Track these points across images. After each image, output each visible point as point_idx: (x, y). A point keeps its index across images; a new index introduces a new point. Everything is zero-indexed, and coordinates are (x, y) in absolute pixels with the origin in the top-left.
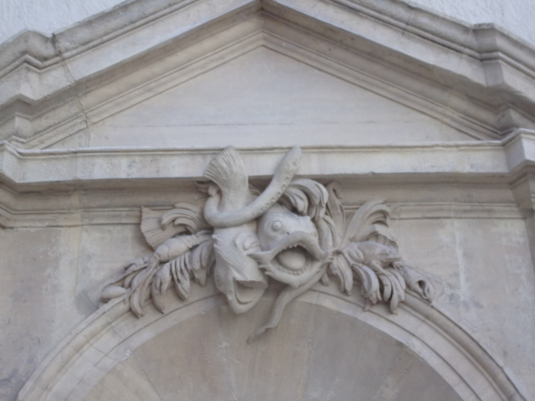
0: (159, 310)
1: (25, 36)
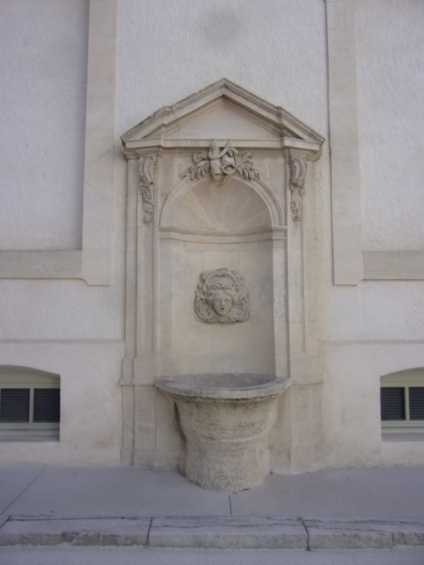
0: (197, 179)
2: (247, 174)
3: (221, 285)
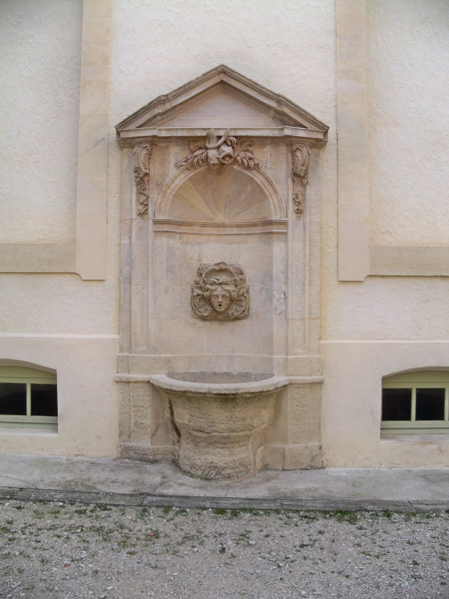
1: (160, 97)
2: (246, 163)
3: (218, 280)
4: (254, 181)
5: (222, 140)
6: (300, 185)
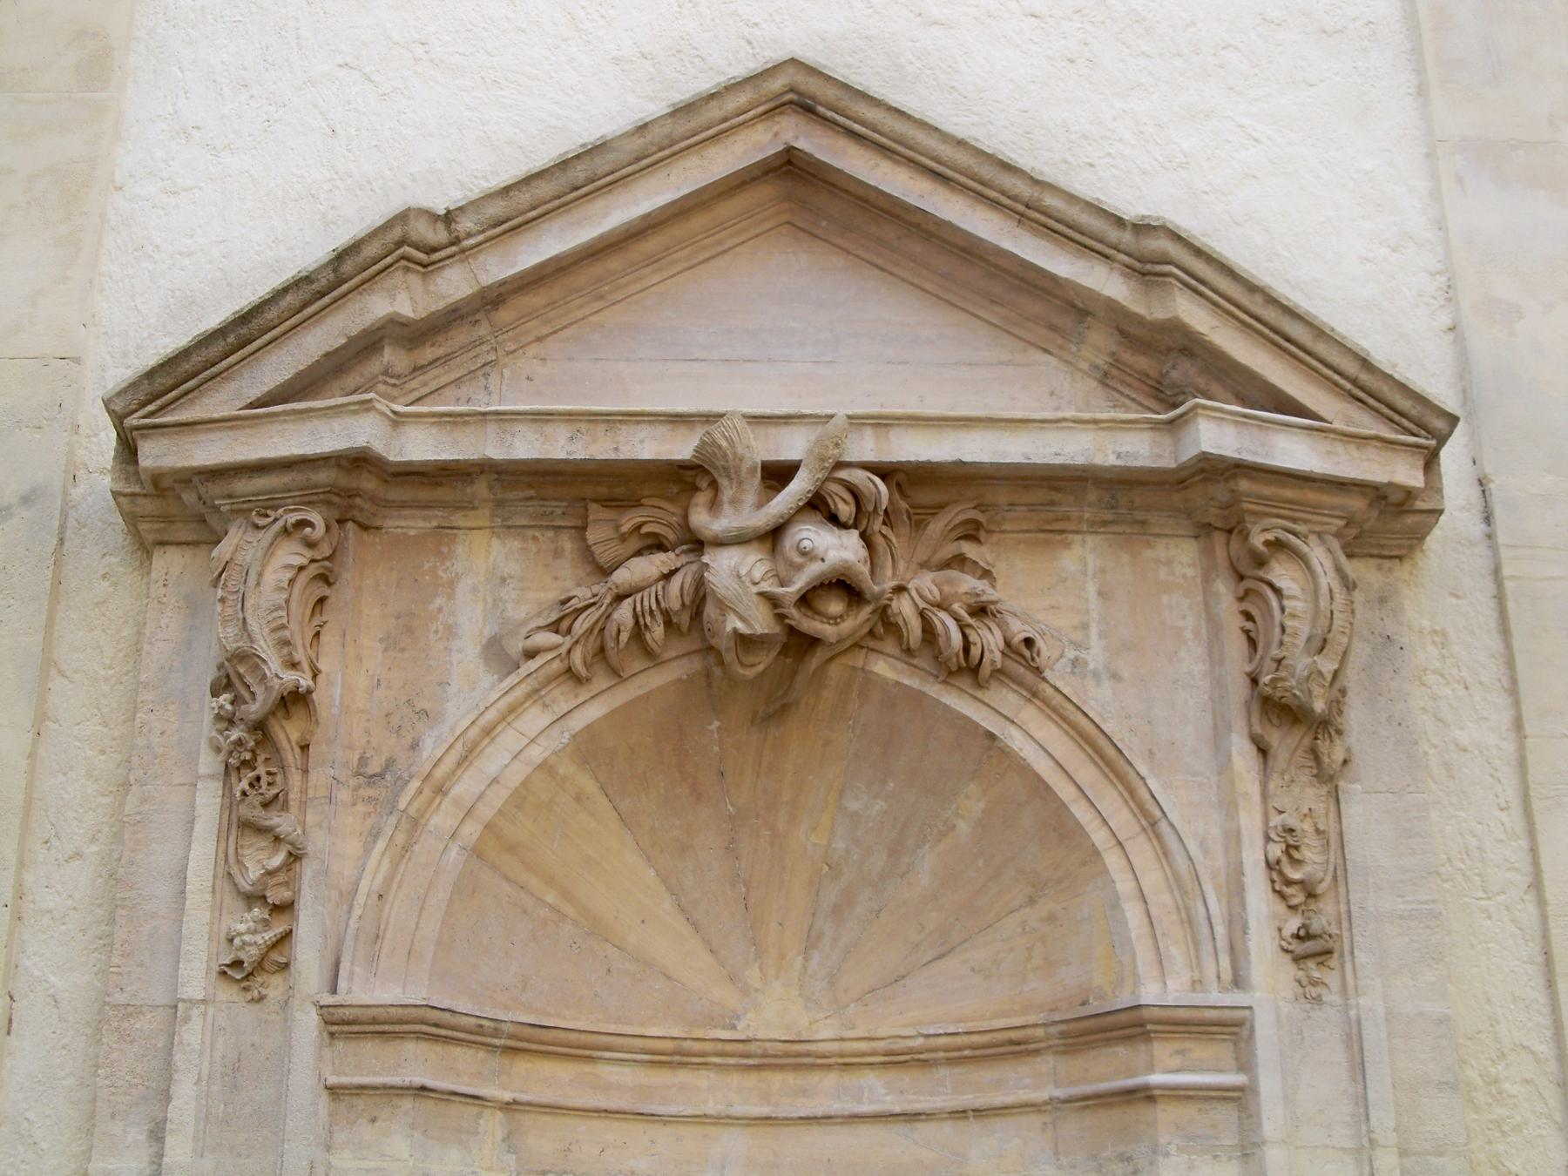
1: (403, 217)
4: (1005, 753)
5: (799, 486)
6: (1304, 777)
